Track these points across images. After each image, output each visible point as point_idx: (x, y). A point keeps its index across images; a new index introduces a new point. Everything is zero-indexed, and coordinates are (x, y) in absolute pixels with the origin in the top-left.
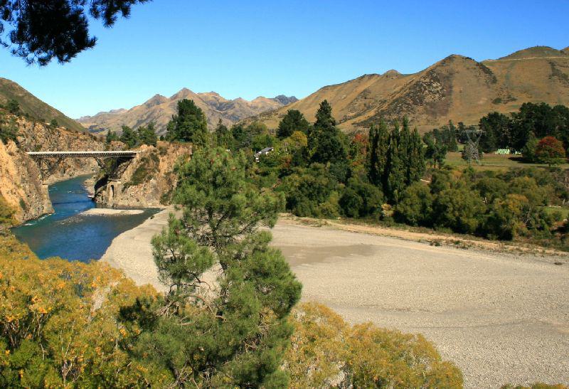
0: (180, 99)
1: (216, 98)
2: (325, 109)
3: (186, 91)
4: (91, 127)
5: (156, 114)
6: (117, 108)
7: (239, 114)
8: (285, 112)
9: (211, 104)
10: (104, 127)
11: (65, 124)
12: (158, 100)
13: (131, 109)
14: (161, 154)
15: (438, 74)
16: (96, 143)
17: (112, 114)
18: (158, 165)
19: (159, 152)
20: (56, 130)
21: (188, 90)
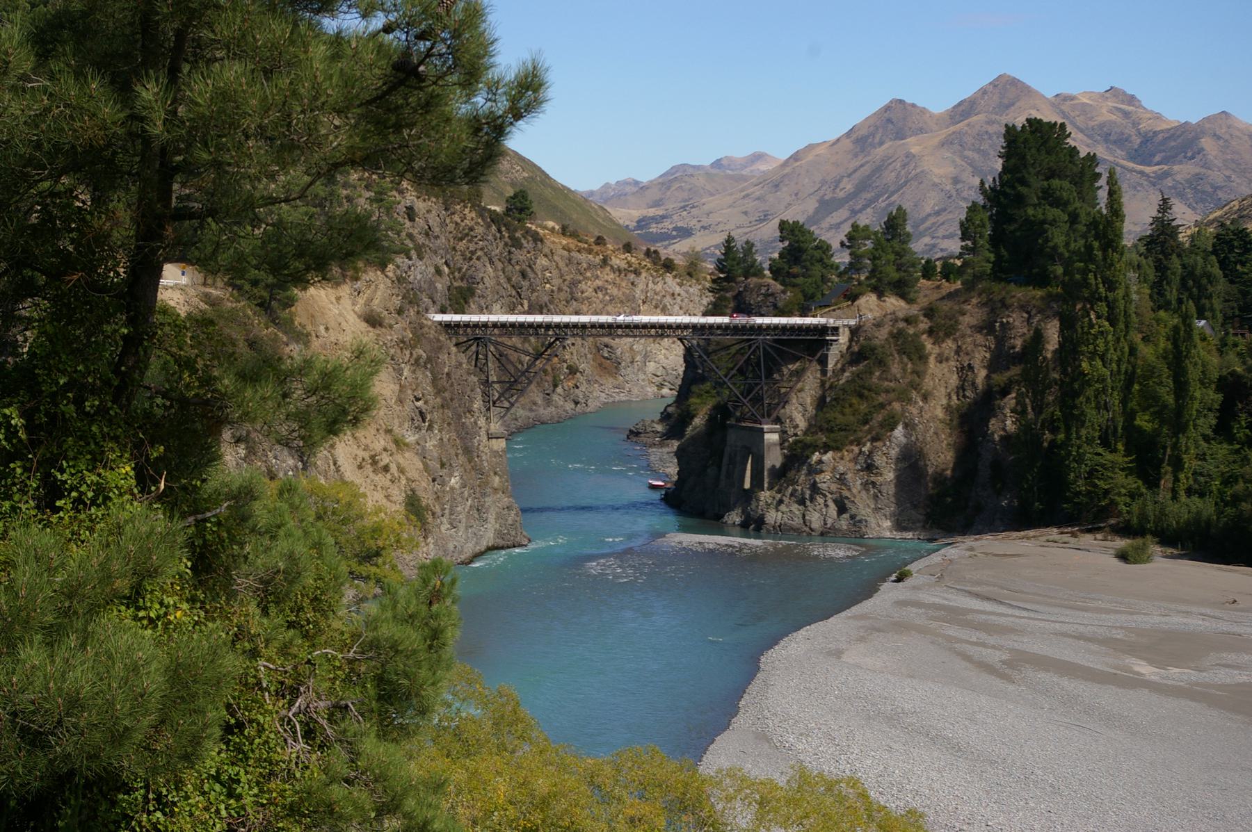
1: (1126, 114)
4: (642, 223)
5: (889, 177)
7: (1216, 177)
10: (693, 223)
11: (554, 212)
13: (796, 157)
14: (931, 332)
15: (218, 165)
16: (671, 282)
18: (919, 374)
19: (924, 324)
20: (528, 231)
21: (1014, 82)
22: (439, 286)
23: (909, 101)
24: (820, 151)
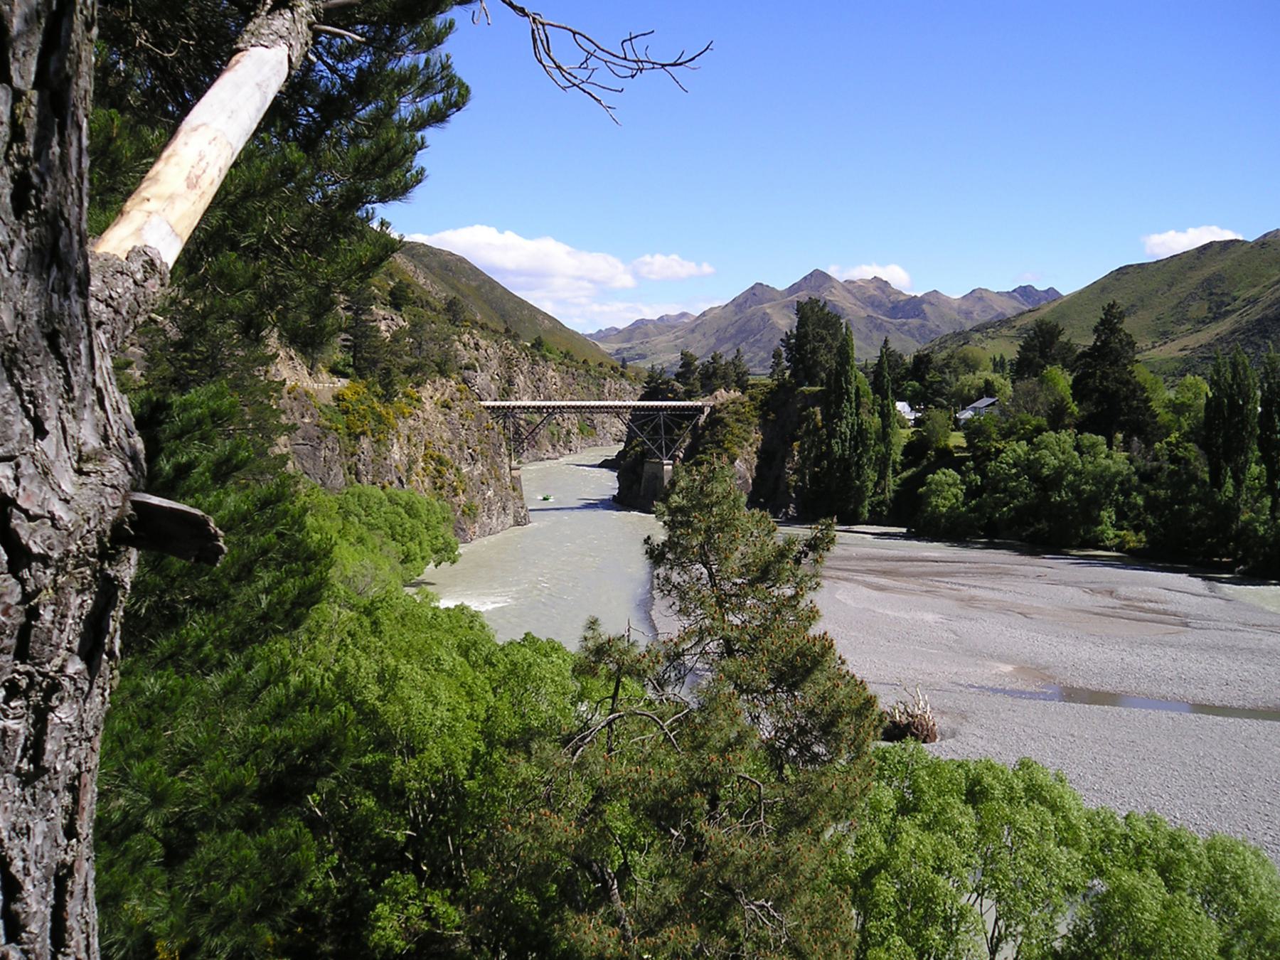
0: (803, 296)
2: (1109, 324)
3: (819, 278)
6: (674, 311)
7: (931, 325)
8: (1029, 320)
9: (872, 304)
12: (758, 293)
13: (704, 314)
17: (664, 324)
22: (493, 386)
23: (1041, 286)
24: (716, 311)
